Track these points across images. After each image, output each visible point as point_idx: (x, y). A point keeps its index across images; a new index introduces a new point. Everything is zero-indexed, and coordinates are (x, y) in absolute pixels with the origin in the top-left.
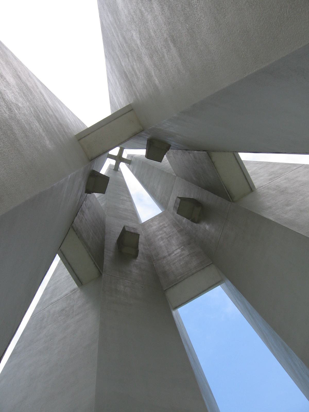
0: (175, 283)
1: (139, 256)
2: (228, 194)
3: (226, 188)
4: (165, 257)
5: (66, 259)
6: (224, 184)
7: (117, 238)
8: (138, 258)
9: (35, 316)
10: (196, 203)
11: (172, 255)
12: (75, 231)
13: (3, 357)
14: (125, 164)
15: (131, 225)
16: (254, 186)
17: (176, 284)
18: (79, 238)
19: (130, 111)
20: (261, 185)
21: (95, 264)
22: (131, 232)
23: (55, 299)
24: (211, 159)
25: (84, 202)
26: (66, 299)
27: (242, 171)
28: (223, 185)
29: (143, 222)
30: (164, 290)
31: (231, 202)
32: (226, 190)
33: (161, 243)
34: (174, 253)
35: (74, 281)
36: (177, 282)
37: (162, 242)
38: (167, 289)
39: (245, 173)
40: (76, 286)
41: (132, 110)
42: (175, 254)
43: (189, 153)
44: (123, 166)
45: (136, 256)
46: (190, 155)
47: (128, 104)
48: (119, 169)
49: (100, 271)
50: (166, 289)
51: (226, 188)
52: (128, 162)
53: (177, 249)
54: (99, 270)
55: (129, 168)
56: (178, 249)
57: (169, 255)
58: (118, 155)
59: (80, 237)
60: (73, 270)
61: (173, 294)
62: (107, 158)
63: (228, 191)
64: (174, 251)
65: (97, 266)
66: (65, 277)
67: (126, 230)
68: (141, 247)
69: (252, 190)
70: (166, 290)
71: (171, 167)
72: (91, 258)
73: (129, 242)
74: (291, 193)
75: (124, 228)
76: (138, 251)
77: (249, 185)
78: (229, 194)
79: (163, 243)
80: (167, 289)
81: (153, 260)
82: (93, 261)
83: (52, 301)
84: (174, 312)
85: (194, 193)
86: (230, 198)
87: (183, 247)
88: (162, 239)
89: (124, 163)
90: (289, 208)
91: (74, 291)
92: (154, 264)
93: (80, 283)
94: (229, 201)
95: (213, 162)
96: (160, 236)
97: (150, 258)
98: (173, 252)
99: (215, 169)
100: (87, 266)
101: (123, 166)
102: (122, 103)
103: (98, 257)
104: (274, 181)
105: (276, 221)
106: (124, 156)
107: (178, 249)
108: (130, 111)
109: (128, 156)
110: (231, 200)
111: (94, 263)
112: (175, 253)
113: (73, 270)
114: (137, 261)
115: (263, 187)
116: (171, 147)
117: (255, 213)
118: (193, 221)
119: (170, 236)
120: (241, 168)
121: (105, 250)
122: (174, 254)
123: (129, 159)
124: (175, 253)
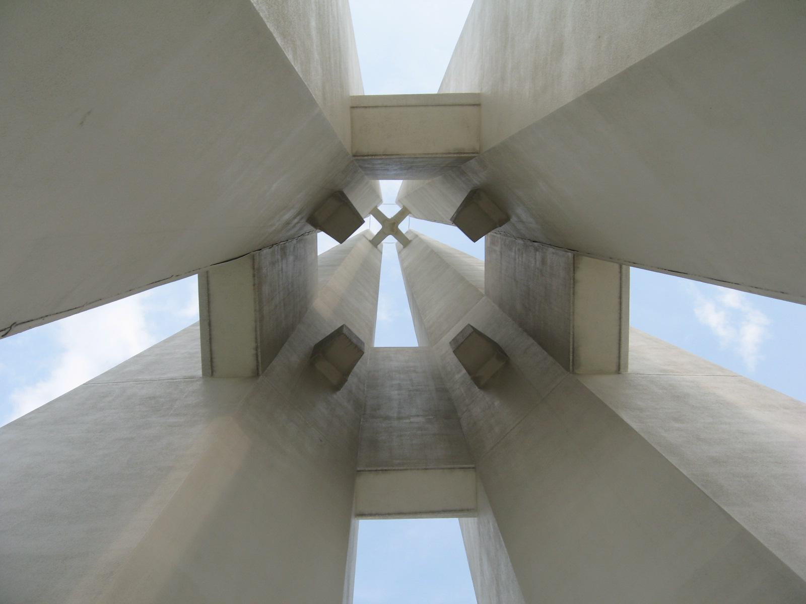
0: (382, 467)
1: (341, 391)
2: (571, 354)
3: (573, 338)
4: (387, 418)
5: (209, 311)
6: (573, 332)
7: (317, 342)
8: (338, 393)
9: (93, 386)
10: (499, 352)
11: (404, 421)
12: (254, 269)
13: (30, 328)
14: (394, 245)
15: (358, 330)
16: (626, 367)
17: (386, 470)
18: (254, 285)
19: (474, 105)
20: (641, 372)
21: (257, 350)
22: (350, 340)
23: (148, 377)
24: (574, 273)
25: (295, 241)
26: (168, 384)
27: (620, 325)
28: (572, 333)
29: (375, 346)
30: (359, 469)
31: (568, 373)
32: (571, 343)
33: (394, 394)
34: (410, 419)
35: (200, 365)
36: (389, 468)
37: (396, 392)
38: (363, 471)
39: (623, 332)
40: (200, 373)
41: (479, 105)
42: (411, 423)
43: (536, 250)
44: (390, 244)
45: (337, 388)
46: (536, 255)
47: (477, 91)
48: (379, 246)
49: (258, 369)
50: (363, 469)
51: (573, 338)
52: (404, 241)
53: (418, 416)
54: (257, 366)
55: (399, 253)
56: (422, 416)
57: (399, 418)
58: (392, 218)
59: (258, 286)
60: (210, 339)
61: (372, 485)
62: (370, 213)
63: (573, 348)
64: (412, 416)
65: (259, 354)
66: (186, 353)
67: (344, 332)
68: (352, 380)
69: (619, 370)
70: (360, 471)
71: (483, 279)
72: (256, 335)
73: (336, 355)
74: (693, 406)
75: (342, 327)
76: (346, 380)
77: (619, 357)
78: (573, 356)
79: (399, 395)
80: (363, 471)
81: (364, 411)
82: (256, 342)
83: (139, 378)
84: (354, 521)
85: (504, 333)
86: (571, 364)
87: (431, 417)
88: (400, 387)
89: (396, 241)
90: (677, 425)
91: (191, 379)
92: (362, 420)
93: (210, 371)
94: (568, 369)
95: (574, 279)
96: (398, 382)
97: (359, 406)
98: (409, 417)
99: (572, 295)
100: (241, 348)
101: (390, 244)
102: (466, 85)
103: (269, 347)
104: (669, 376)
105: (642, 435)
106: (403, 227)
107: (422, 416)
108: (474, 105)
109: (409, 232)
110: (571, 368)
111: (256, 349)
112: (412, 420)
113: (210, 339)
114: (335, 396)
115: (642, 376)
116: (506, 227)
117: (606, 406)
118: (476, 380)
119: (417, 390)
120: (620, 318)
121: (286, 345)
122: (407, 421)
123: (409, 237)
124: (412, 420)
